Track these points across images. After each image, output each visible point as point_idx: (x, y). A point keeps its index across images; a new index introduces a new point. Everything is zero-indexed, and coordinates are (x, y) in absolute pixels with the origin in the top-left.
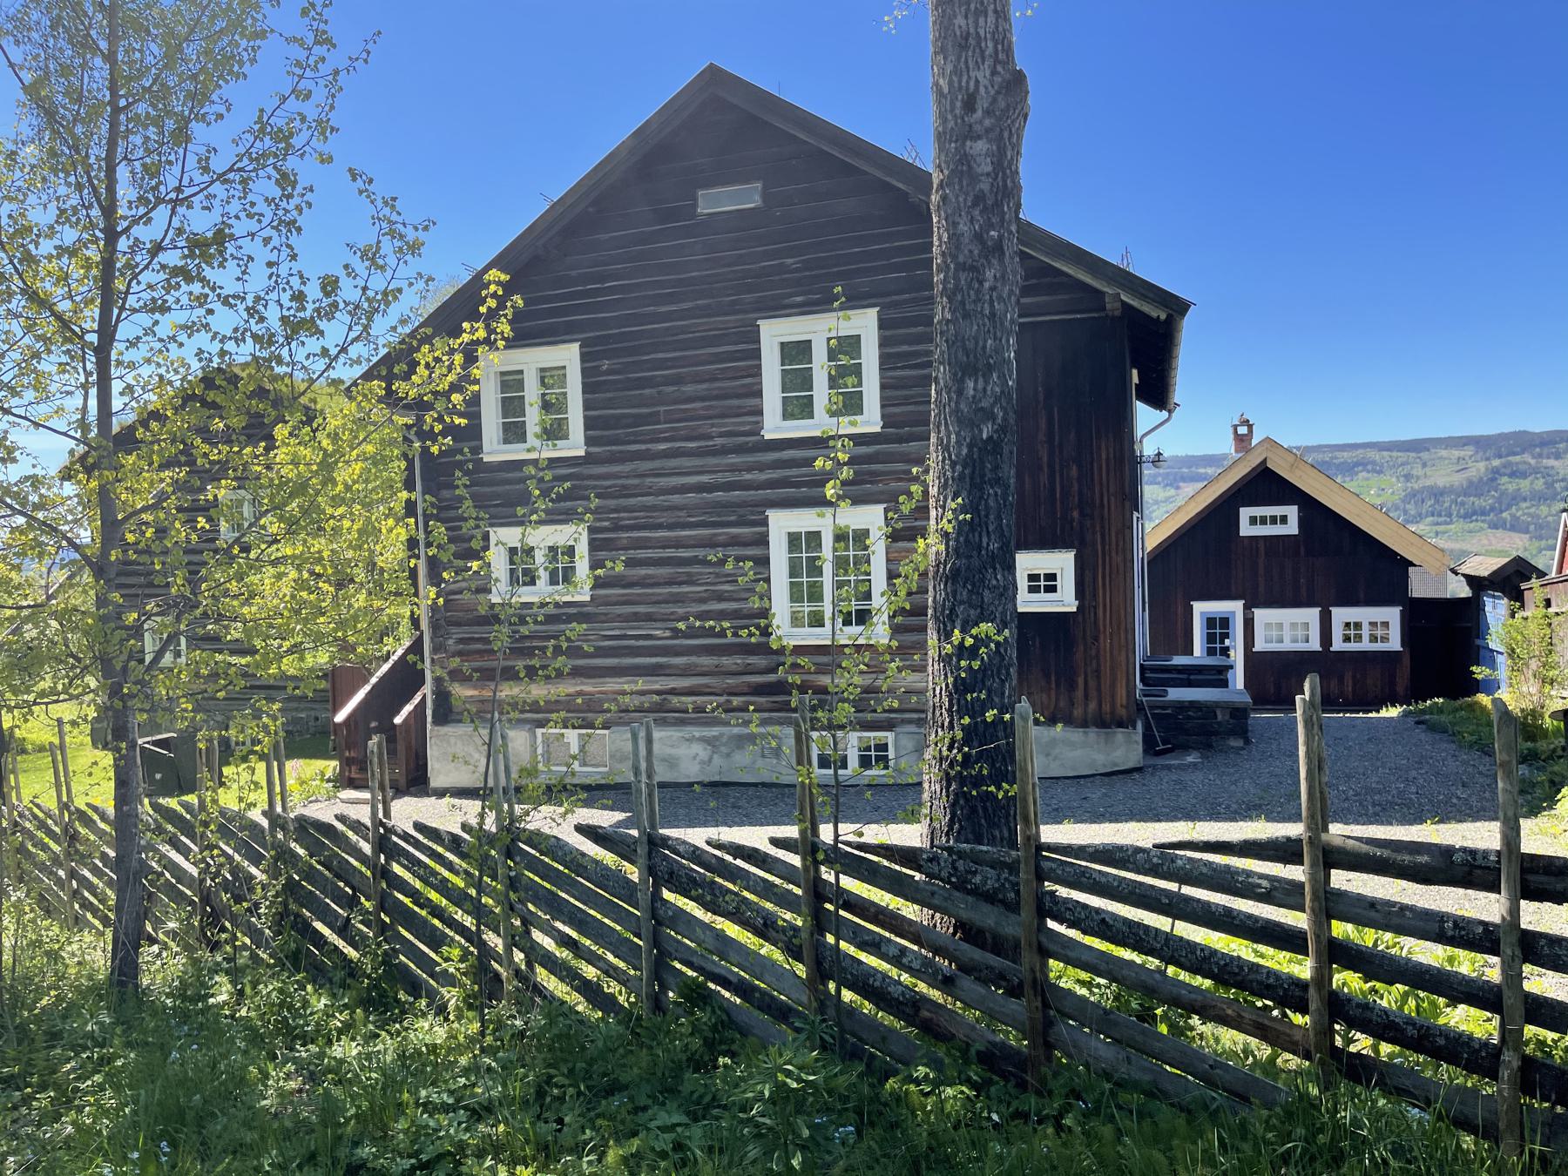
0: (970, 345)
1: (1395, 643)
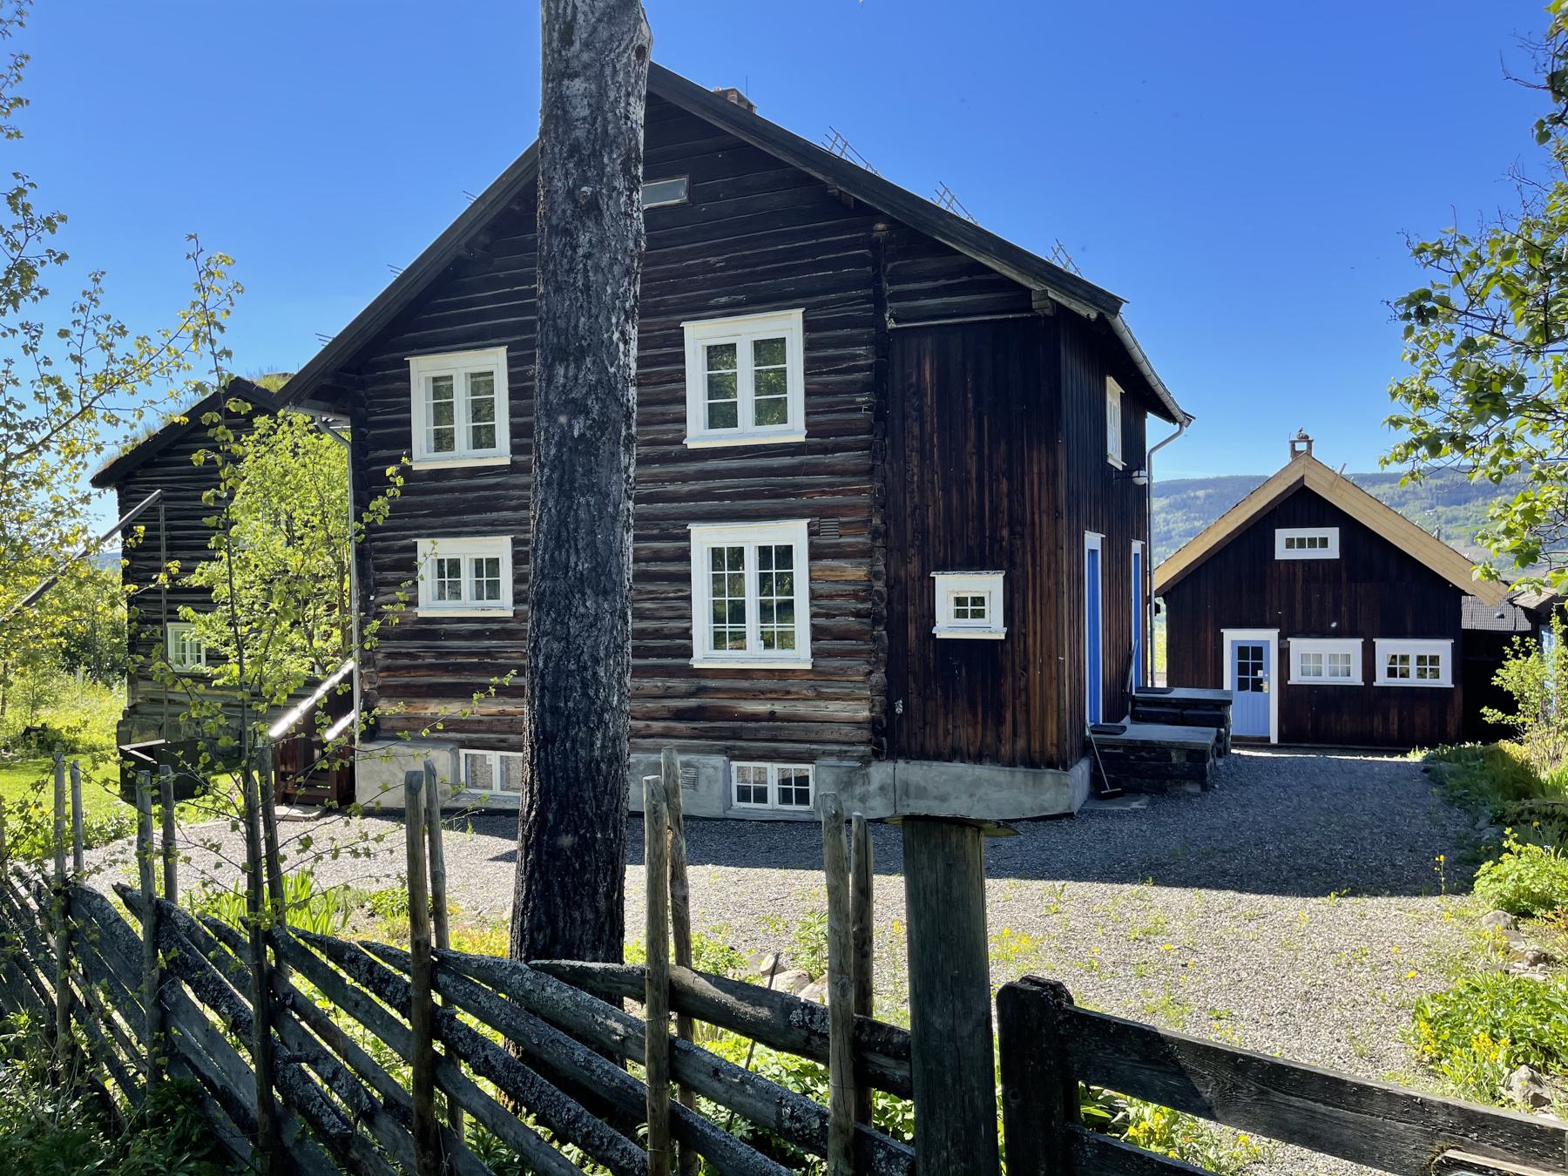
0: (561, 323)
1: (1445, 680)
